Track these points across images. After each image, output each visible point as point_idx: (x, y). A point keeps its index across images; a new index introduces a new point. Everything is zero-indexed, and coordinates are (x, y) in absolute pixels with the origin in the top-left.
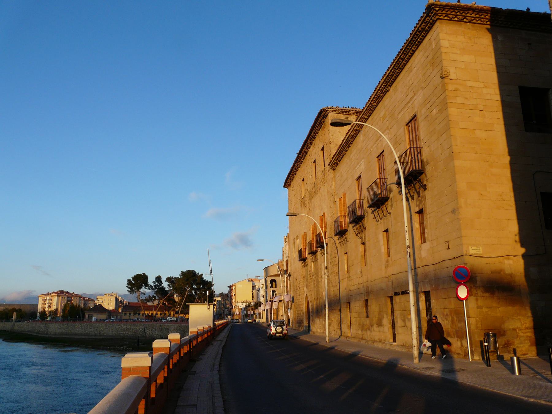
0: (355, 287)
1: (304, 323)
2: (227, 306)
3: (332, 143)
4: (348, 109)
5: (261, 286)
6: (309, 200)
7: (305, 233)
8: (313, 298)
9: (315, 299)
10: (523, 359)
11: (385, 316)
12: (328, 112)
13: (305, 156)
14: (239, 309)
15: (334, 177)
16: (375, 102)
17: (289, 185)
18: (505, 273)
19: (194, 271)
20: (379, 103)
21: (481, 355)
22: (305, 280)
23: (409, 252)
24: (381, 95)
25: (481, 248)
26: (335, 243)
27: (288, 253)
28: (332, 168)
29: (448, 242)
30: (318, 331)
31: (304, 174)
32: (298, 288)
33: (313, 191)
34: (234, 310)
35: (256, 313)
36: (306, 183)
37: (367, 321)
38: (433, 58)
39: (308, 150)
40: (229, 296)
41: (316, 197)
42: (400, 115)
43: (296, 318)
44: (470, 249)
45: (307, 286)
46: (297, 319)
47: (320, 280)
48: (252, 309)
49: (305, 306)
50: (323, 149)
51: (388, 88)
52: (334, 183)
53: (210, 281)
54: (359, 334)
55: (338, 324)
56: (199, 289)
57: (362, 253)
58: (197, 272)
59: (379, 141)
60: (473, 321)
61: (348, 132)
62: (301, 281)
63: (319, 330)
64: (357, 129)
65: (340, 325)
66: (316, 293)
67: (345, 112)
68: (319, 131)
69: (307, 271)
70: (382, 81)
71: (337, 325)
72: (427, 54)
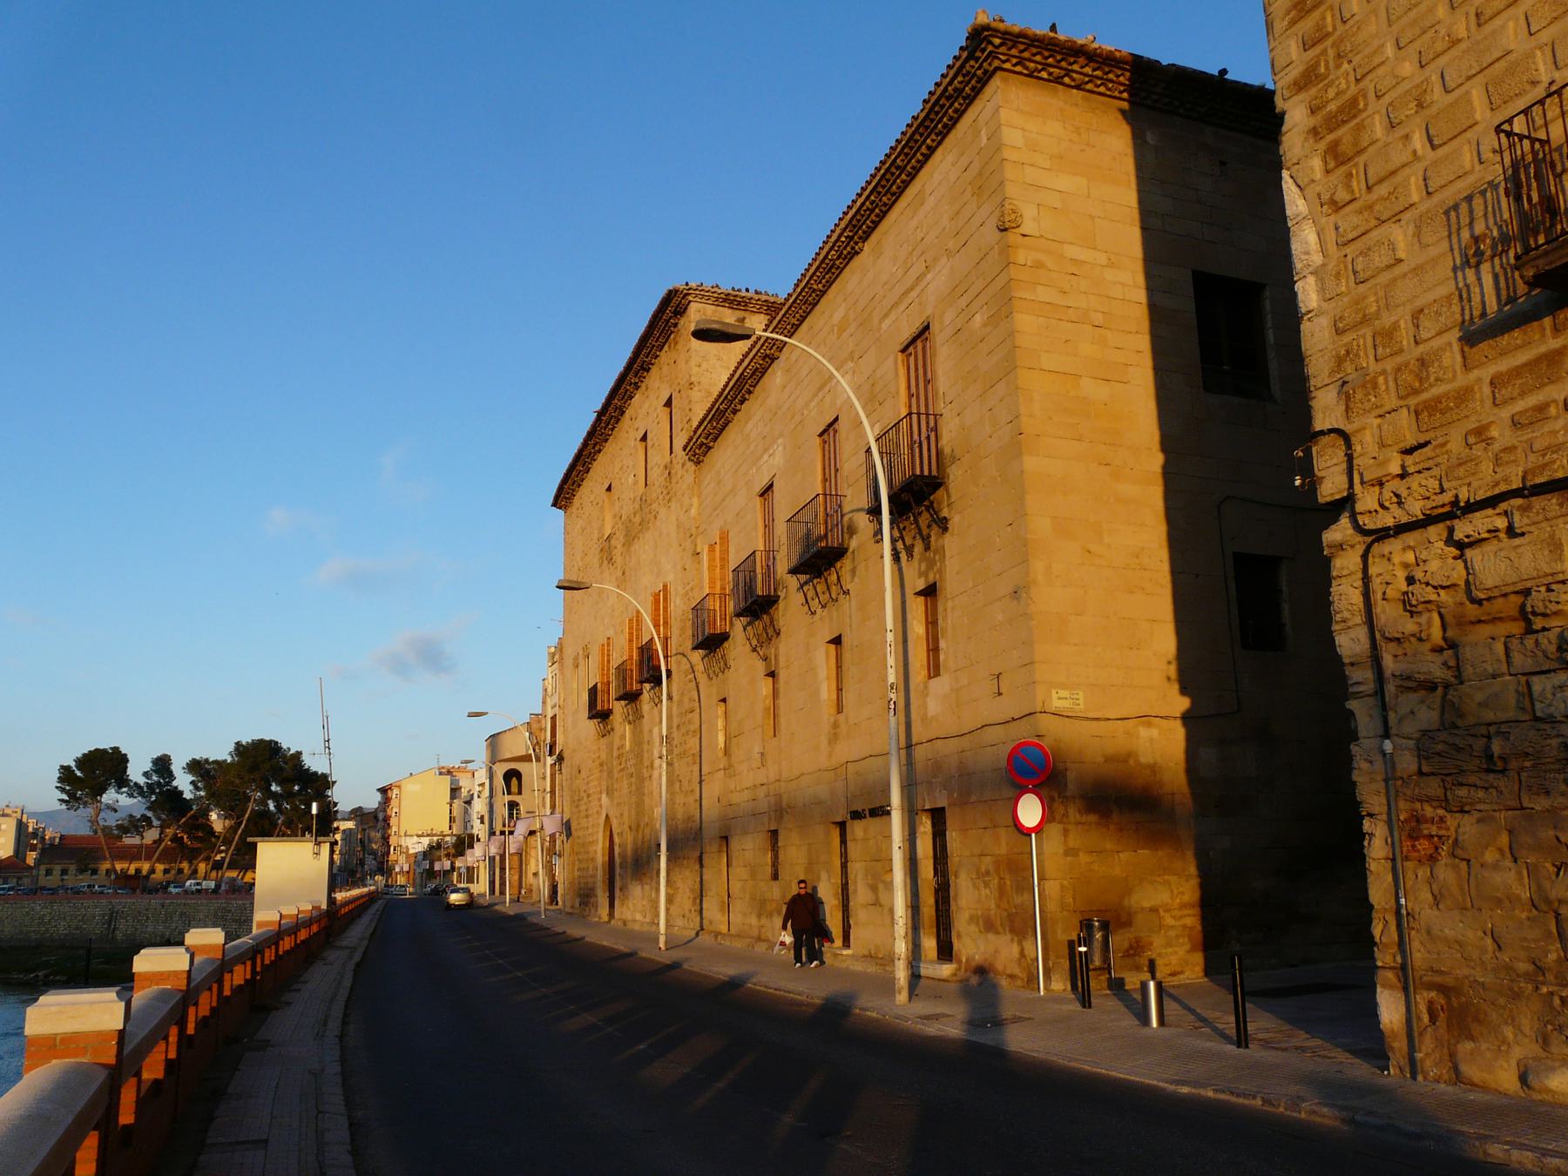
0: (746, 795)
1: (596, 896)
2: (374, 846)
3: (696, 388)
4: (744, 293)
5: (478, 789)
7: (609, 638)
8: (626, 827)
9: (630, 827)
12: (690, 298)
13: (618, 420)
14: (408, 856)
15: (697, 481)
16: (820, 282)
17: (569, 500)
18: (1138, 762)
19: (276, 743)
20: (830, 283)
21: (1069, 978)
24: (837, 262)
25: (1081, 695)
26: (694, 672)
32: (585, 795)
33: (637, 519)
34: (392, 857)
35: (459, 868)
40: (381, 816)
42: (887, 322)
43: (576, 881)
44: (1054, 696)
45: (610, 792)
46: (579, 883)
47: (646, 775)
48: (448, 855)
49: (603, 848)
50: (669, 403)
51: (856, 243)
52: (695, 501)
53: (323, 774)
54: (751, 926)
55: (695, 899)
56: (288, 795)
58: (285, 746)
59: (827, 389)
60: (1053, 887)
61: (742, 361)
64: (768, 352)
65: (698, 901)
66: (633, 812)
68: (660, 351)
69: (610, 746)
70: (843, 225)
71: (691, 901)
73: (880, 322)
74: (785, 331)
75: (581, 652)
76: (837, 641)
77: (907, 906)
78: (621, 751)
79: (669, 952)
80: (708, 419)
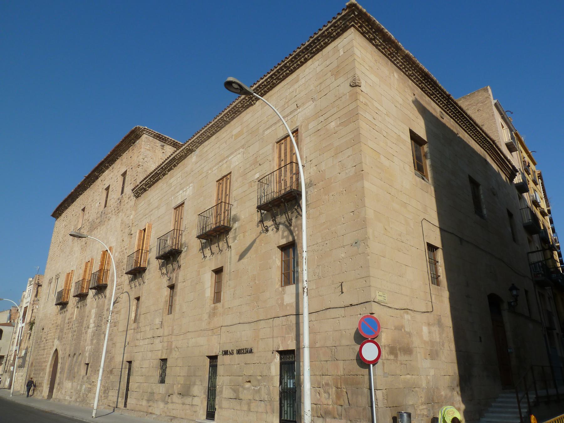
1: (43, 387)
3: (141, 167)
6: (88, 232)
10: (18, 362)
11: (198, 382)
12: (144, 132)
15: (135, 205)
20: (233, 118)
22: (59, 330)
23: (307, 287)
24: (240, 109)
27: (31, 298)
28: (136, 194)
29: (342, 285)
30: (66, 398)
31: (87, 202)
33: (98, 221)
36: (88, 212)
37: (162, 389)
38: (338, 67)
39: (101, 174)
41: (100, 228)
42: (268, 131)
44: (377, 294)
45: (60, 339)
47: (84, 331)
50: (124, 175)
51: (253, 101)
57: (167, 298)
59: (225, 162)
61: (135, 188)
62: (50, 331)
63: (67, 398)
64: (191, 148)
66: (72, 348)
67: (162, 139)
72: (328, 62)
73: (264, 131)
74: (260, 93)
75: (54, 277)
76: (138, 299)
77: (303, 403)
78: (70, 320)
79: (97, 419)
80: (149, 177)
